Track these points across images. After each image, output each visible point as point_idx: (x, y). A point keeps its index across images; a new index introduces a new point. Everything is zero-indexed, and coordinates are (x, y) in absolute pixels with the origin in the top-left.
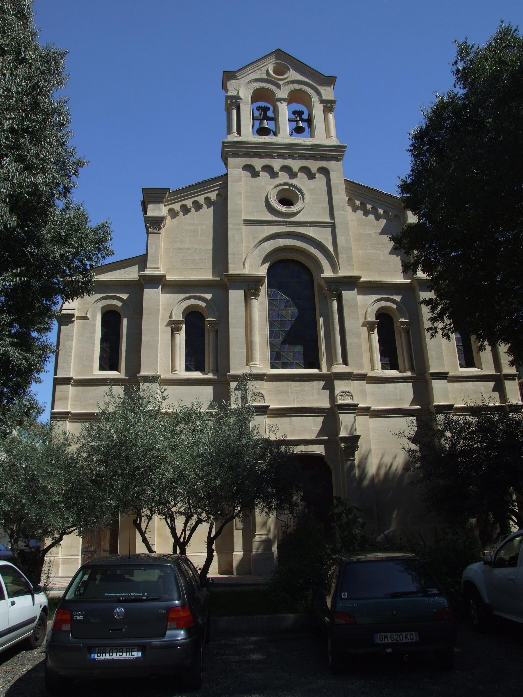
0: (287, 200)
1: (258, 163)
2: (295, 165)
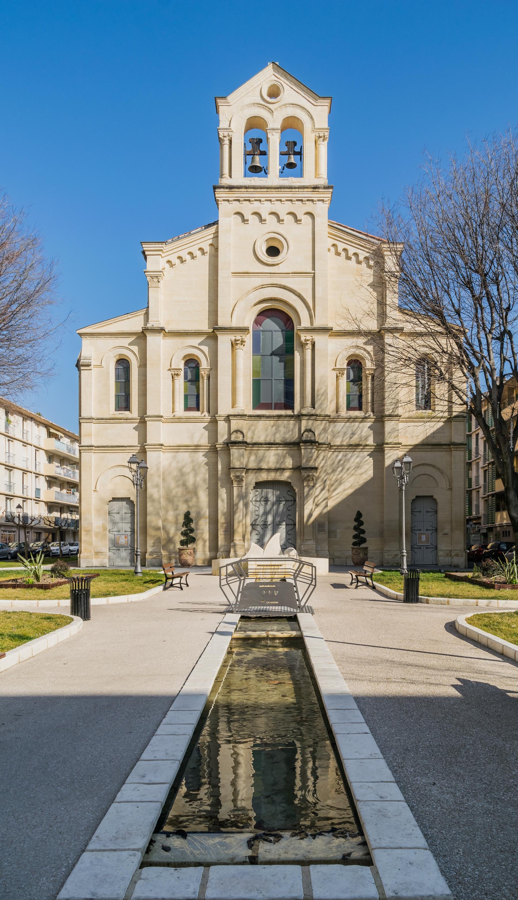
0: (273, 251)
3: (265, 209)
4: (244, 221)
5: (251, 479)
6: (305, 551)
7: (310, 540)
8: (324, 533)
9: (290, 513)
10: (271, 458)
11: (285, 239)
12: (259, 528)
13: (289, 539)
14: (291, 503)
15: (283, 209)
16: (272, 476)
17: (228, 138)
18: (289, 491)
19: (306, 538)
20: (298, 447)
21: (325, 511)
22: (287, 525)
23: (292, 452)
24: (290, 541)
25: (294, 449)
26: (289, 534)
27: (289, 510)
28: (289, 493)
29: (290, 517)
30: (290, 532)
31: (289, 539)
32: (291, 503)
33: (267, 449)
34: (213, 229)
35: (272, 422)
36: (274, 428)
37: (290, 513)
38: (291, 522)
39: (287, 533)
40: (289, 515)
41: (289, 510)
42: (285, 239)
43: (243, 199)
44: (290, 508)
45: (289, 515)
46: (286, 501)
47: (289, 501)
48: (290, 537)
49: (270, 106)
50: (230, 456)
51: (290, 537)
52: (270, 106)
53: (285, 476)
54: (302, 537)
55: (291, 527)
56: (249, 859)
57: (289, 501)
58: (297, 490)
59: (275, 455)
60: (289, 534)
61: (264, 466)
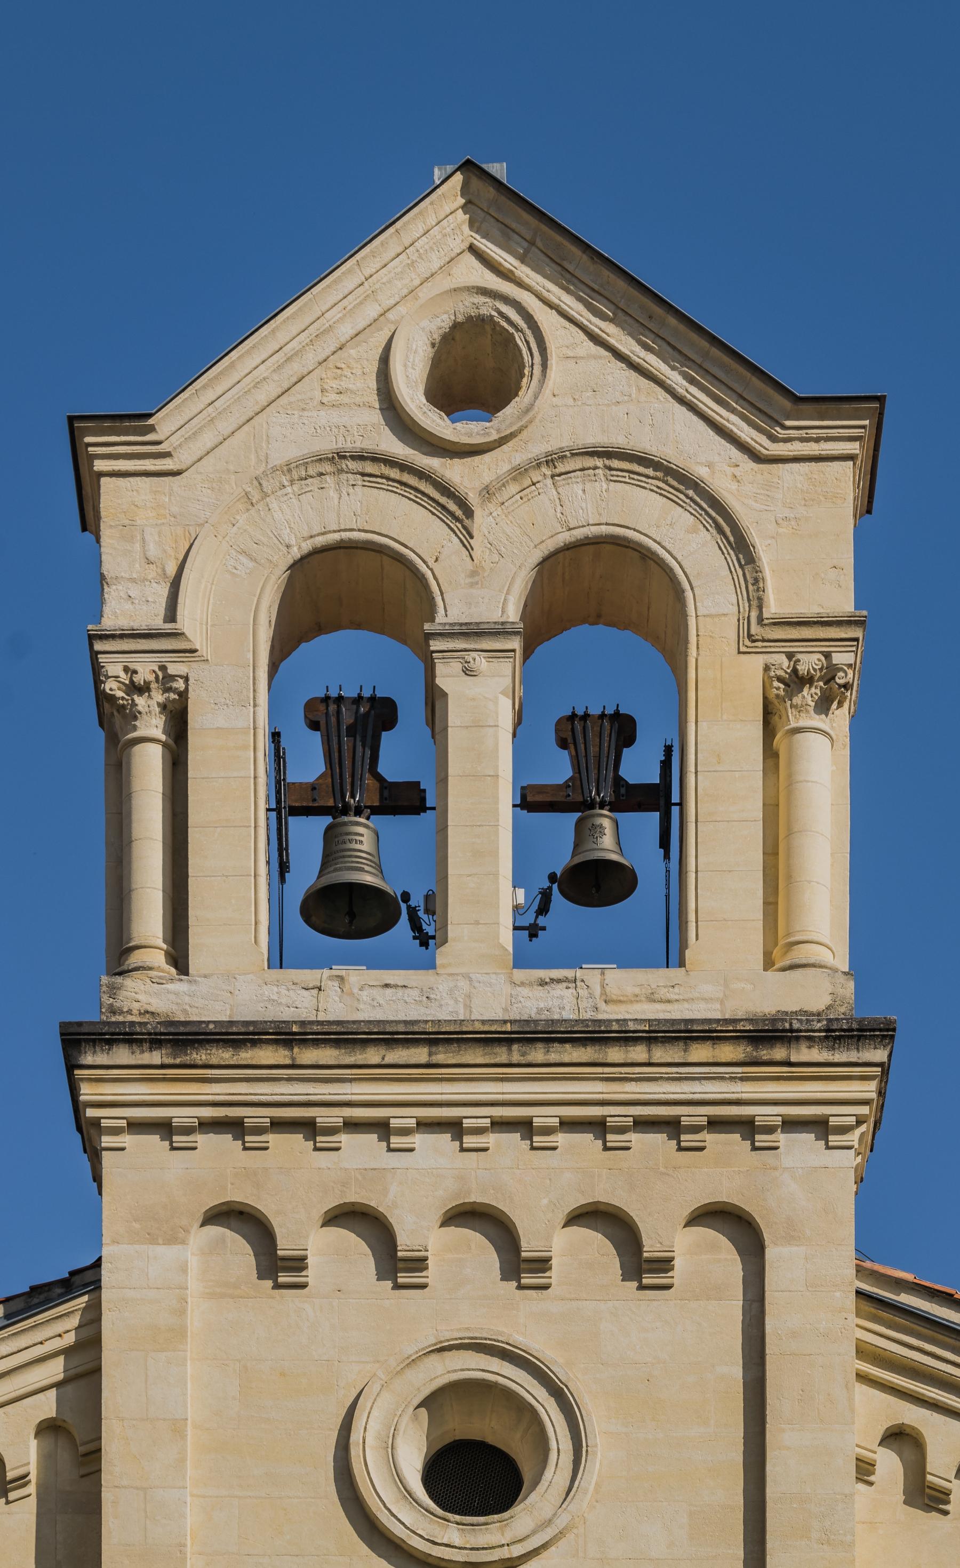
0: (477, 1472)
1: (294, 1184)
2: (538, 1185)
3: (416, 1182)
4: (278, 1266)
11: (558, 1393)
15: (538, 1185)
17: (158, 697)
42: (558, 1393)
43: (262, 1116)
49: (454, 471)
52: (454, 471)
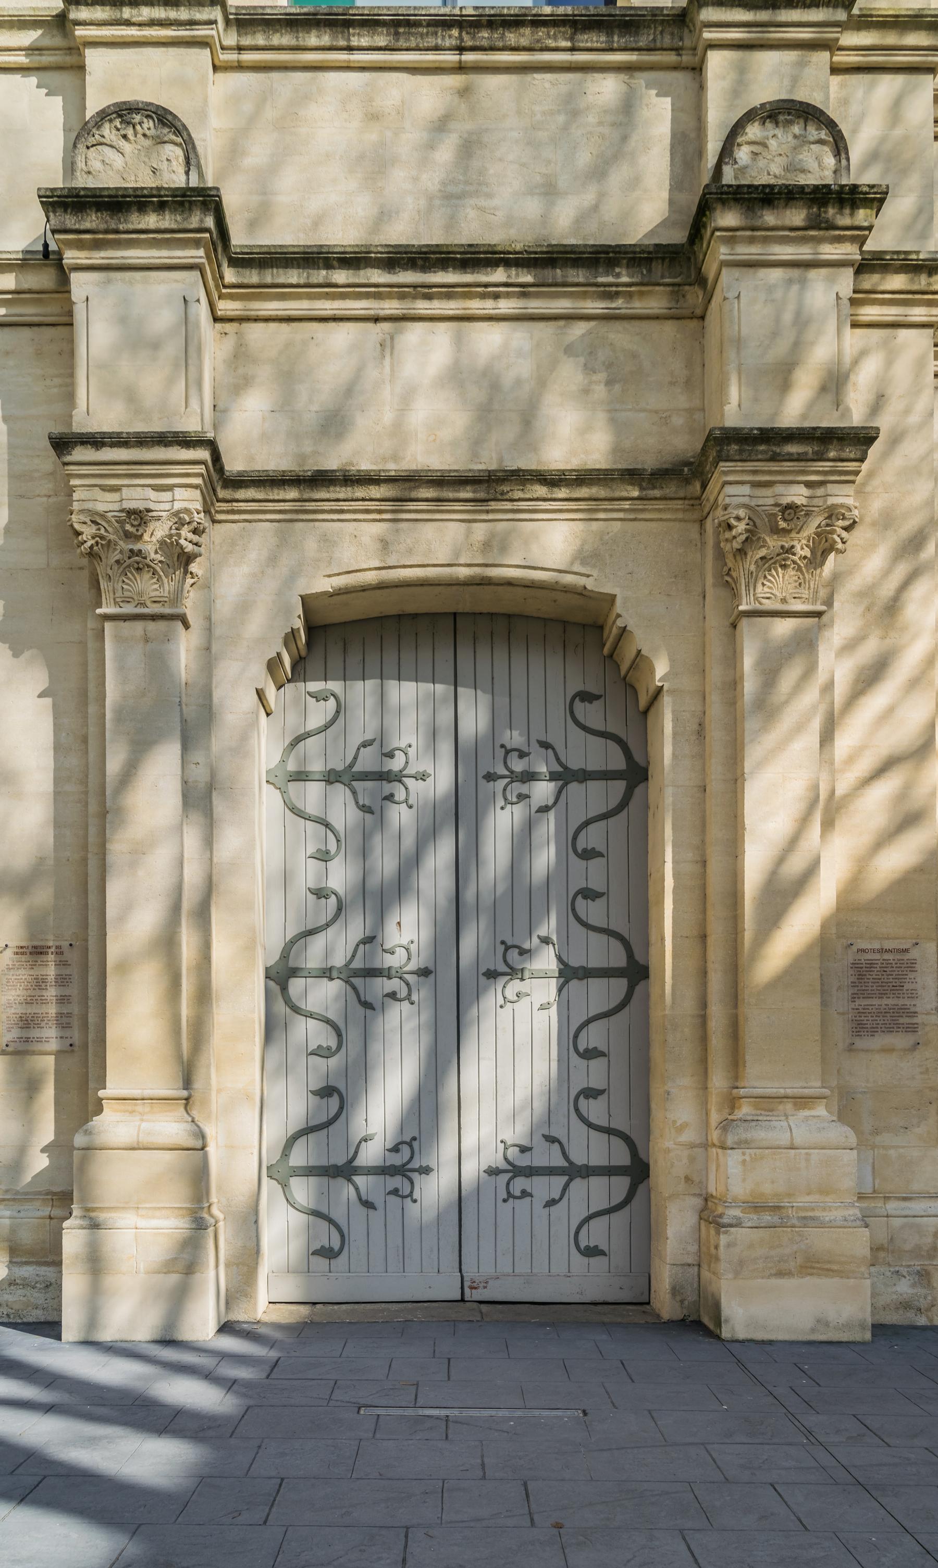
5: (252, 581)
6: (756, 1207)
7: (802, 1101)
8: (900, 1040)
9: (594, 874)
10: (416, 388)
12: (322, 995)
13: (590, 1093)
14: (596, 797)
16: (440, 546)
18: (585, 697)
19: (760, 1079)
20: (677, 292)
21: (897, 859)
22: (568, 973)
23: (621, 337)
24: (595, 1110)
25: (639, 306)
26: (590, 1054)
27: (588, 855)
28: (591, 714)
29: (593, 912)
30: (593, 1037)
31: (590, 1093)
32: (596, 797)
33: (391, 307)
34: (503, 968)
35: (428, 95)
36: (445, 154)
37: (594, 874)
38: (600, 952)
39: (575, 1045)
40: (588, 894)
41: (588, 855)
44: (592, 838)
45: (588, 894)
46: (564, 776)
47: (584, 776)
48: (594, 1074)
50: (71, 374)
51: (594, 1074)
53: (550, 544)
54: (718, 1081)
55: (600, 994)
56: (651, 88)
57: (584, 776)
58: (661, 668)
59: (456, 376)
60: (590, 1054)
61: (359, 451)
